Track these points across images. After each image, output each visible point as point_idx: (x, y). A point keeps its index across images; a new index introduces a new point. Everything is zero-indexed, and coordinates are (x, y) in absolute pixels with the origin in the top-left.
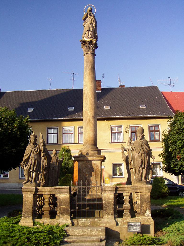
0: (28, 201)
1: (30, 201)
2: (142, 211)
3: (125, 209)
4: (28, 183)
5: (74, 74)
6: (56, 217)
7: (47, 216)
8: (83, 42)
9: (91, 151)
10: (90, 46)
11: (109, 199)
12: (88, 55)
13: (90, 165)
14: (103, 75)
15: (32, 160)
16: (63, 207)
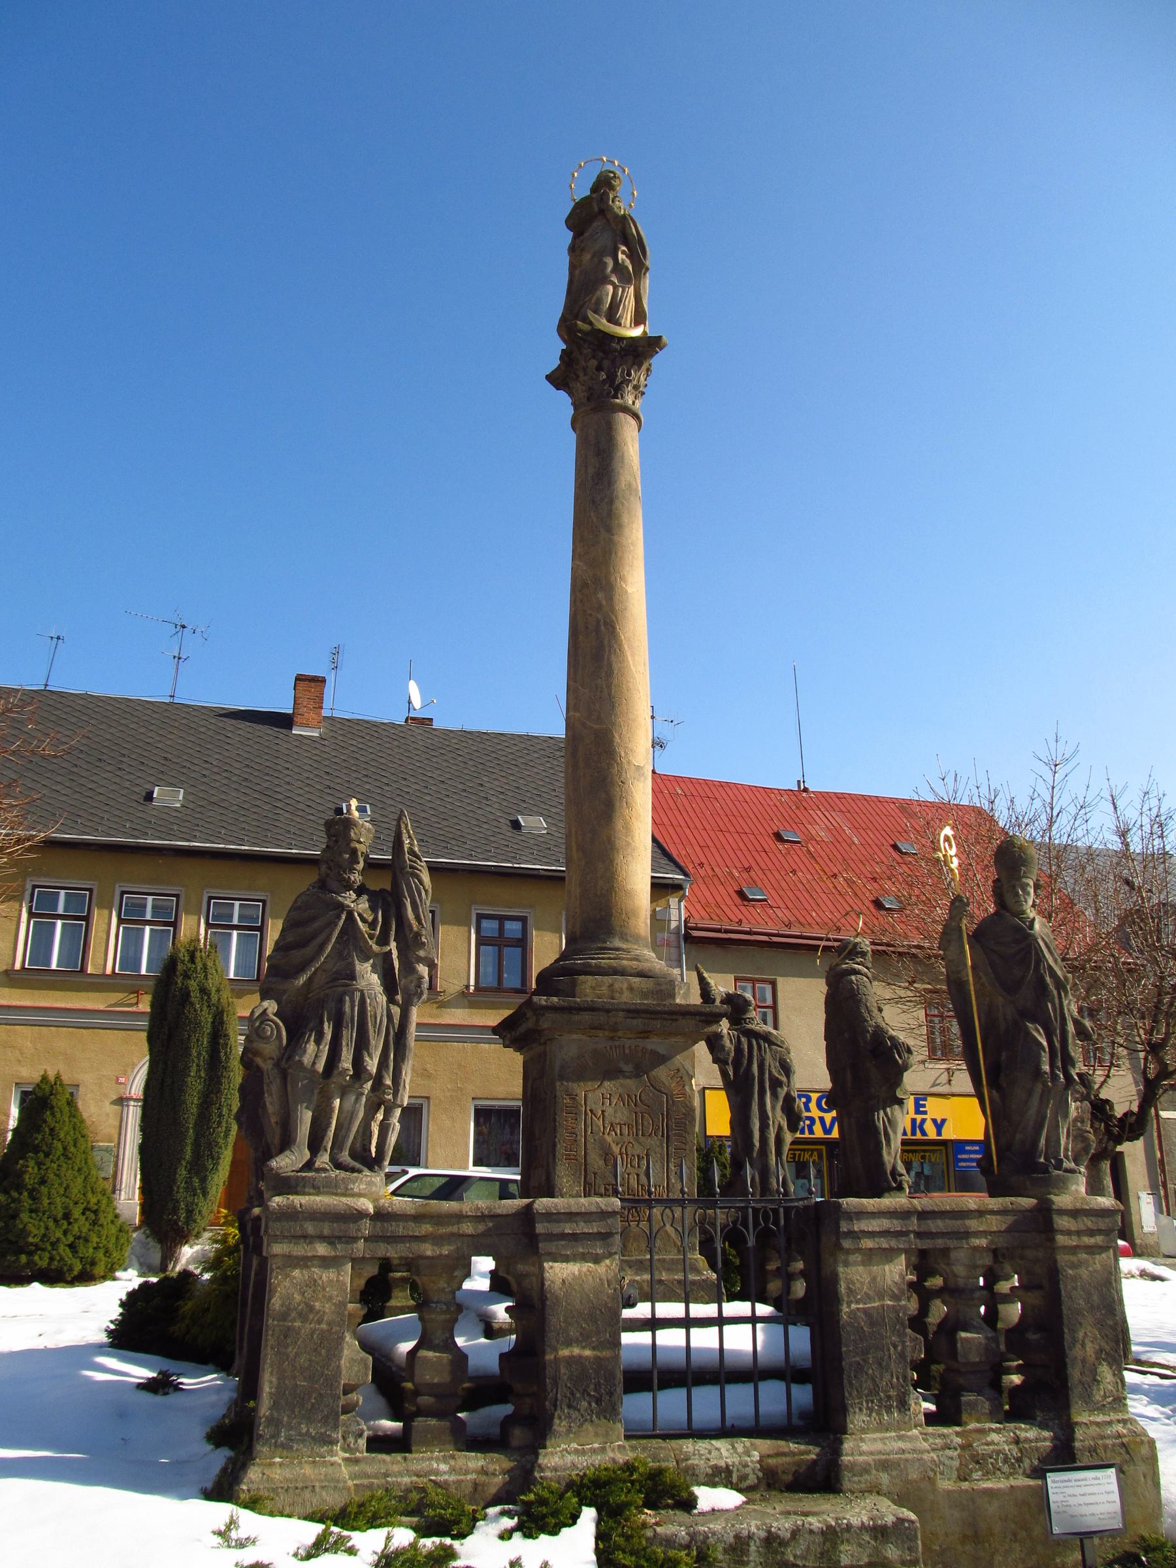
5: (184, 627)
14: (336, 652)
16: (576, 1351)
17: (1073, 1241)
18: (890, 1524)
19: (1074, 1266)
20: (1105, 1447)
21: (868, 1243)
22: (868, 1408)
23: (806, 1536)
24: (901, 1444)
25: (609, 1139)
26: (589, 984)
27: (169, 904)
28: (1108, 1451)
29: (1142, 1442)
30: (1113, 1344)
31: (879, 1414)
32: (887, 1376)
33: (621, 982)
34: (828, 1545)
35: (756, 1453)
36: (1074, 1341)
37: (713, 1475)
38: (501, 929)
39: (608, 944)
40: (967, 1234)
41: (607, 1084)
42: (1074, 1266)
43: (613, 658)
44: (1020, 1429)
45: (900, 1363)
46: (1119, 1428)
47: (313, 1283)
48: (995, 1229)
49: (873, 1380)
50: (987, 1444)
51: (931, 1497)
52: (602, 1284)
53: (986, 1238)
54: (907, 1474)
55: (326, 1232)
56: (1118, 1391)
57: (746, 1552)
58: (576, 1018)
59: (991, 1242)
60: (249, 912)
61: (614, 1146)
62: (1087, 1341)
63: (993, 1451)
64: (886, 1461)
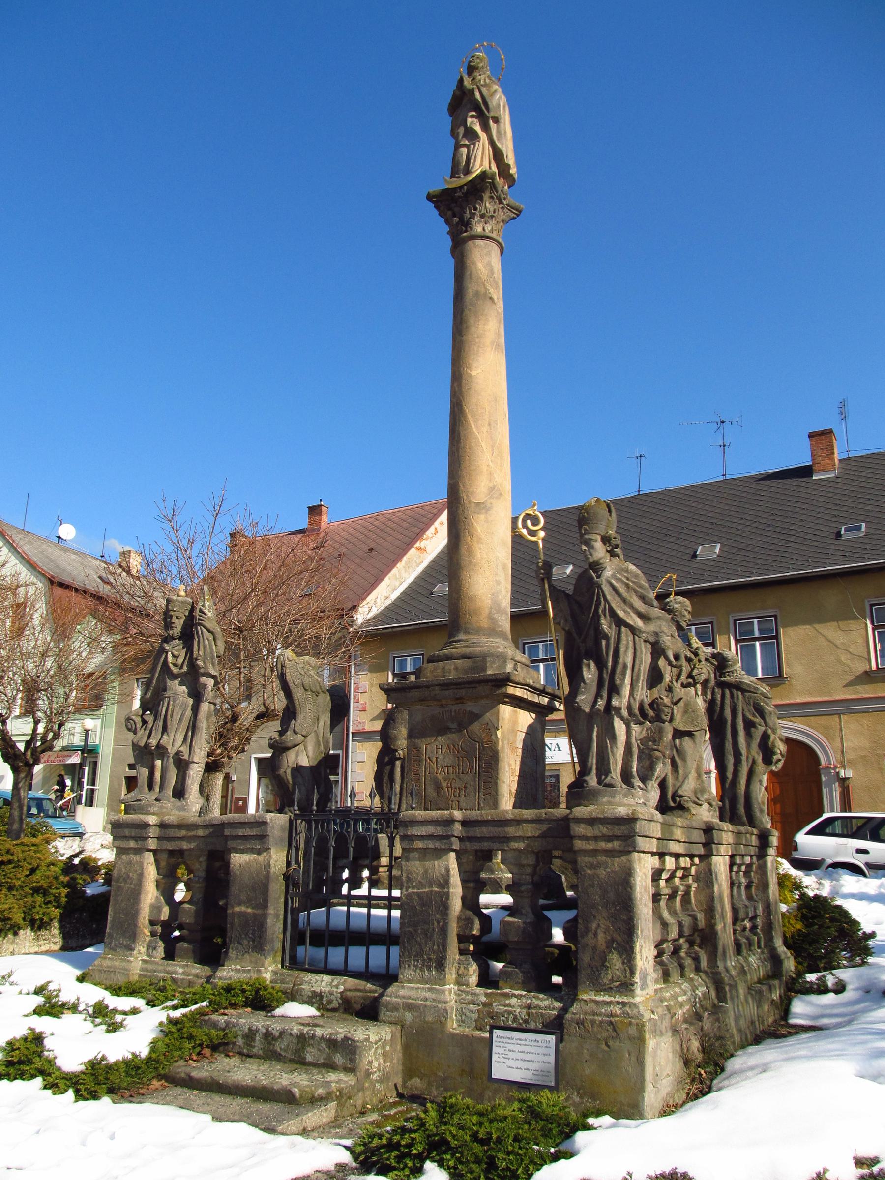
5: (723, 422)
14: (843, 405)
16: (243, 909)
17: (591, 846)
18: (339, 1040)
19: (592, 866)
20: (593, 1022)
21: (419, 844)
22: (414, 966)
23: (288, 1037)
24: (428, 995)
25: (440, 777)
26: (429, 669)
27: (706, 630)
28: (595, 1025)
29: (630, 1023)
30: (626, 936)
31: (422, 970)
32: (430, 944)
33: (450, 665)
34: (300, 1045)
35: (342, 987)
36: (587, 930)
37: (312, 997)
39: (456, 638)
40: (507, 839)
41: (439, 738)
42: (592, 866)
43: (461, 428)
44: (537, 998)
45: (441, 935)
46: (617, 1010)
47: (130, 863)
48: (530, 835)
49: (420, 946)
50: (505, 1006)
51: (440, 1036)
52: (261, 868)
53: (524, 842)
54: (425, 1016)
55: (133, 834)
56: (626, 977)
57: (254, 1040)
58: (410, 695)
59: (528, 845)
60: (767, 626)
61: (443, 782)
62: (599, 931)
63: (506, 1011)
64: (411, 1004)
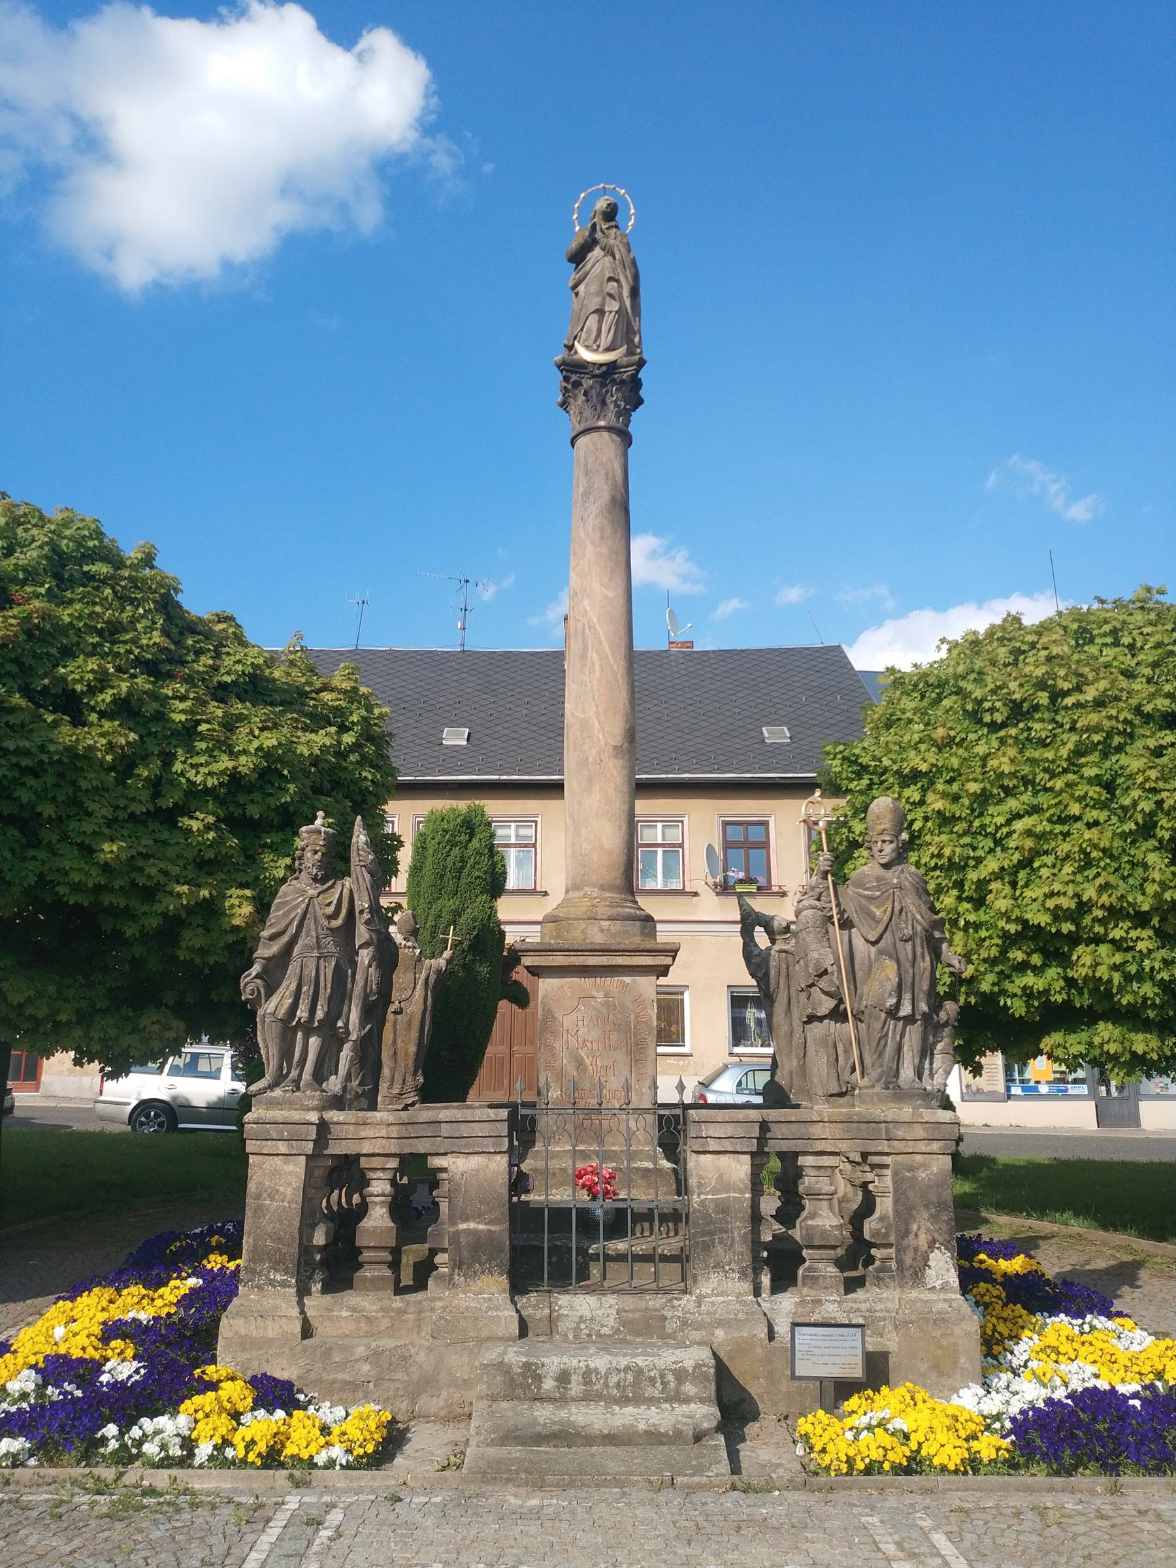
0: (278, 1191)
1: (289, 1191)
2: (908, 1261)
3: (809, 1247)
4: (277, 1093)
6: (430, 1283)
7: (383, 1278)
8: (572, 369)
9: (607, 923)
10: (607, 392)
11: (727, 1188)
12: (594, 436)
13: (601, 995)
15: (302, 962)
16: (472, 1225)
38: (746, 835)
